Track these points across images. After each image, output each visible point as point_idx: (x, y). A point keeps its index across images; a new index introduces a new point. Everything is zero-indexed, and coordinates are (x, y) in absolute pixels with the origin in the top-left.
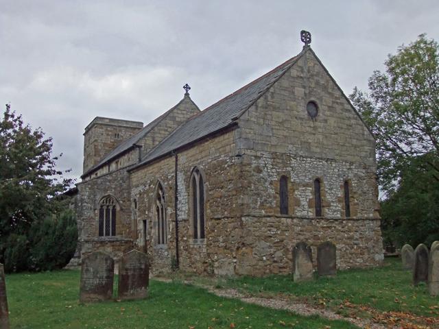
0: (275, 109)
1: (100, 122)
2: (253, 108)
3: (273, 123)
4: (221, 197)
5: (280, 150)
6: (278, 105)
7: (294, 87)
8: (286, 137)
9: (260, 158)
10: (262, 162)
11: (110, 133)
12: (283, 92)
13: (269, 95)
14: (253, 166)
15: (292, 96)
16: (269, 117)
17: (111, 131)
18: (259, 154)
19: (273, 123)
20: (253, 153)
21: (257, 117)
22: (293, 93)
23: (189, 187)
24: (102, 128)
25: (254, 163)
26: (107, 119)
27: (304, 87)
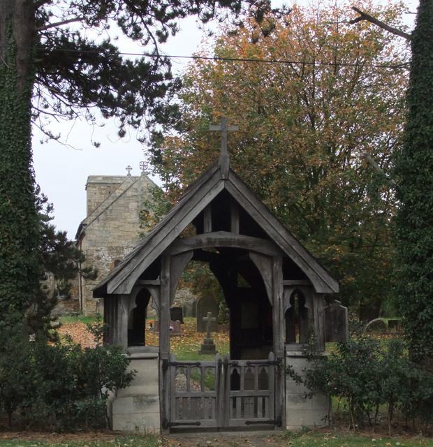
0: (112, 220)
1: (93, 181)
2: (96, 221)
3: (111, 229)
4: (6, 279)
5: (114, 245)
6: (115, 217)
7: (128, 203)
8: (120, 236)
9: (99, 250)
10: (101, 253)
11: (103, 192)
12: (119, 208)
13: (108, 212)
14: (95, 256)
15: (127, 209)
16: (108, 225)
17: (104, 189)
18: (99, 248)
19: (111, 229)
20: (95, 248)
21: (98, 227)
22: (128, 207)
23: (239, 244)
24: (95, 187)
25: (95, 254)
26: (100, 177)
27: (138, 202)
